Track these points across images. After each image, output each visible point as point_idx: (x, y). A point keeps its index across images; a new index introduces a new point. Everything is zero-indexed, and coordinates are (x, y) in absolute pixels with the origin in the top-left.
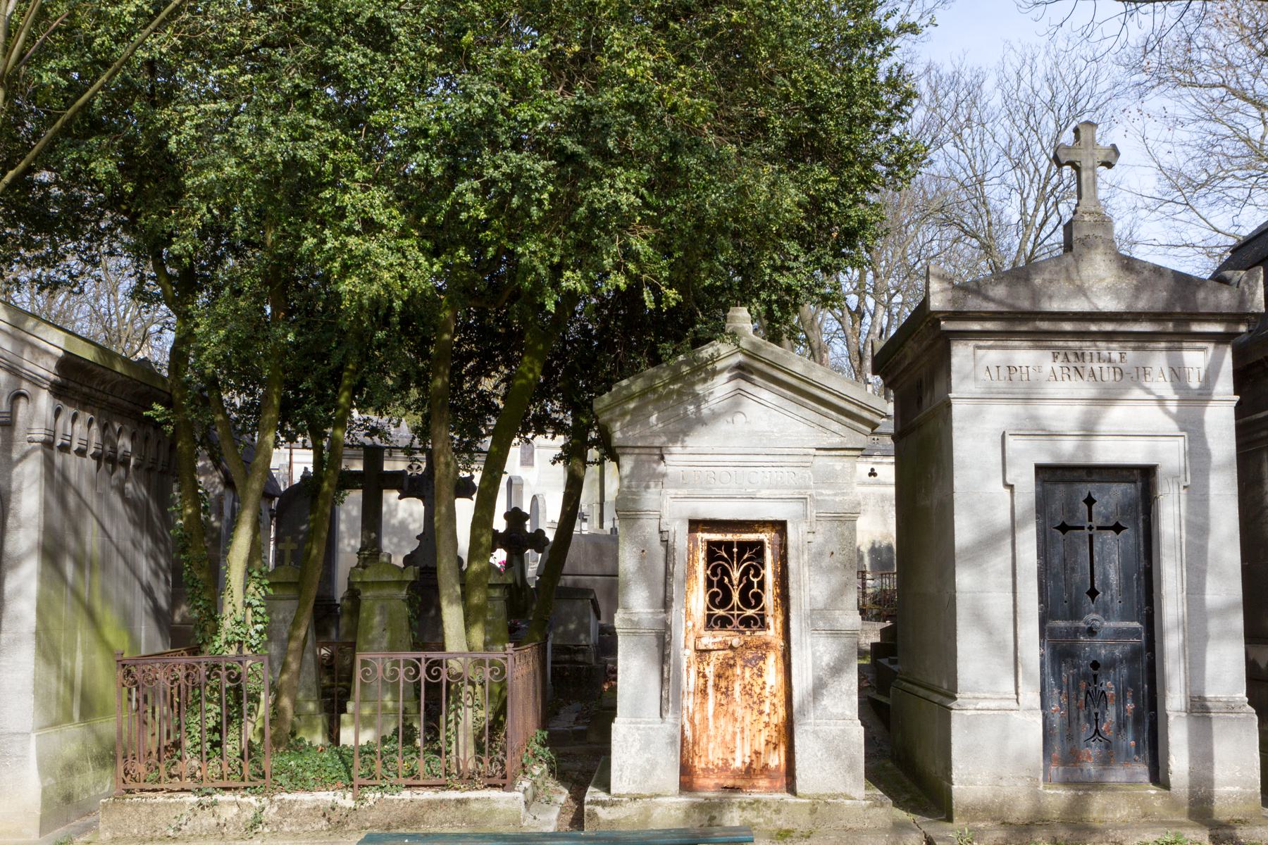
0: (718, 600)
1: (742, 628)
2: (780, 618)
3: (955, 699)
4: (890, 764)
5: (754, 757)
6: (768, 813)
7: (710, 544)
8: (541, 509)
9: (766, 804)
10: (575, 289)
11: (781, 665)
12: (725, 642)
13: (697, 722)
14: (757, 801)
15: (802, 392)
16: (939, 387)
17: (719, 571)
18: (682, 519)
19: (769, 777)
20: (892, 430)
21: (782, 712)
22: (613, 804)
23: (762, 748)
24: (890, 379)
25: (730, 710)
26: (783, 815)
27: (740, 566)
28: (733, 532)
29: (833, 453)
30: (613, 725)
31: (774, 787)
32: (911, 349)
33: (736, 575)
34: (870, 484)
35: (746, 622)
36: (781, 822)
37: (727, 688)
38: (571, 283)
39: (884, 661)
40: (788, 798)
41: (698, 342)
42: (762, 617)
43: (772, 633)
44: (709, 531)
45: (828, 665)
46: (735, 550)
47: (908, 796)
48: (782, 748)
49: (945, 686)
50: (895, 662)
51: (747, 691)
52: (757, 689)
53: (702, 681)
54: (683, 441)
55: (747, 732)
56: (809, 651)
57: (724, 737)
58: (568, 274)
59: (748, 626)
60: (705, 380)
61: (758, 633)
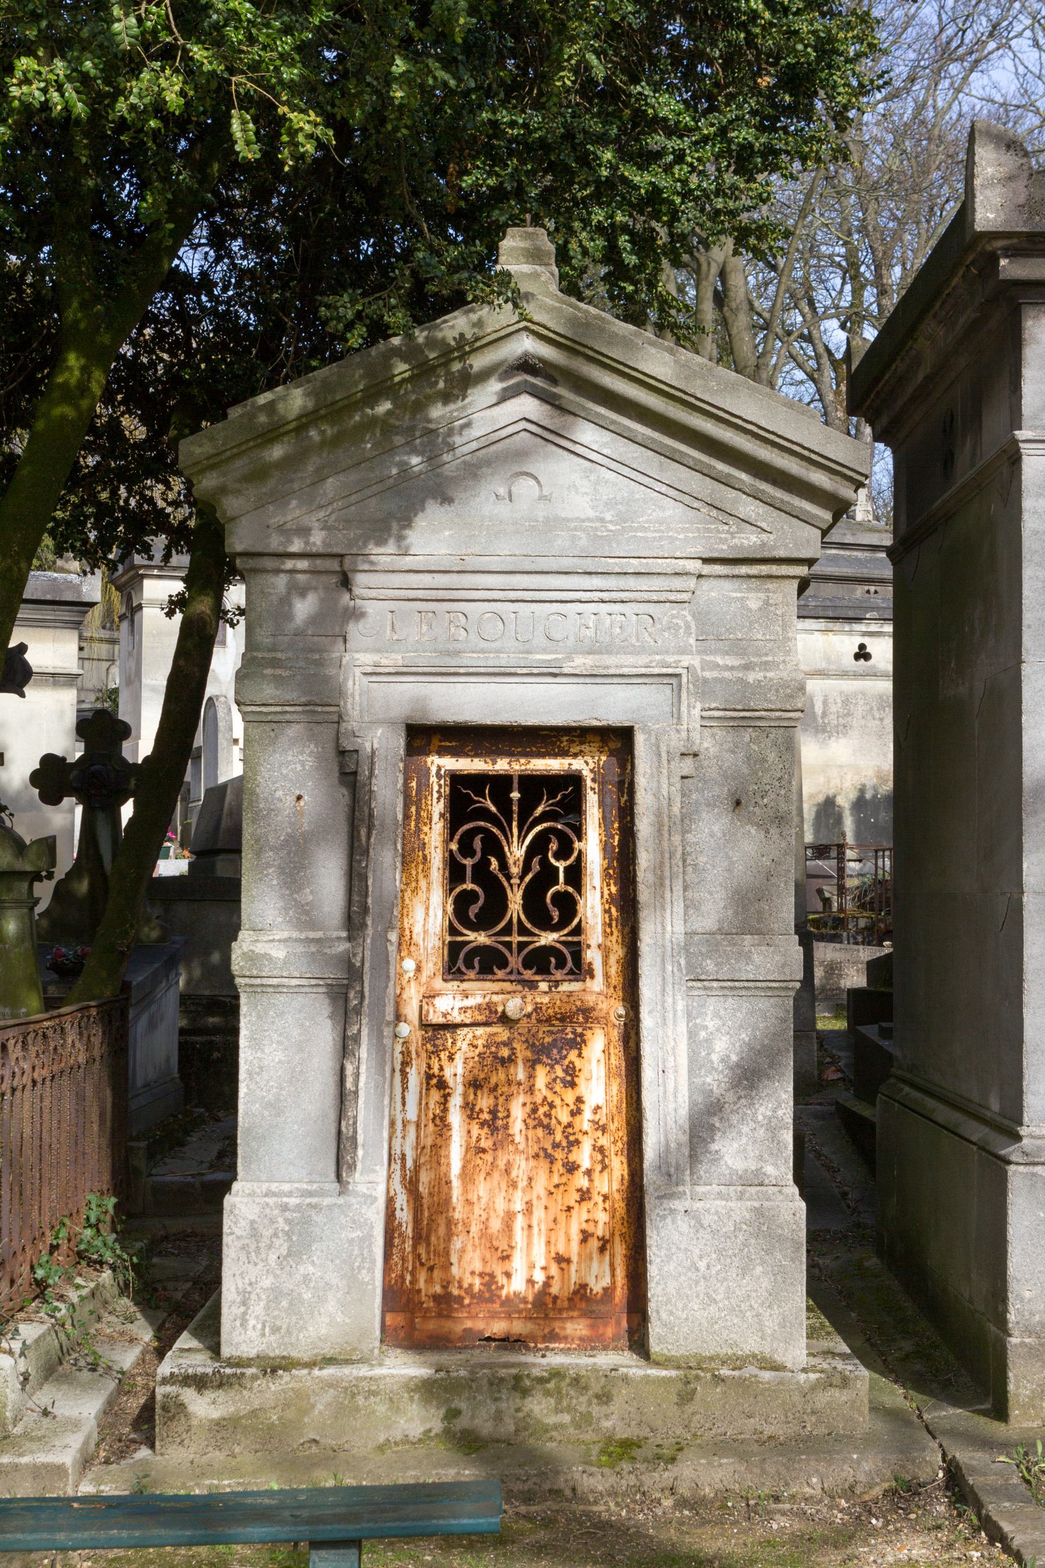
0: (473, 910)
1: (528, 974)
2: (618, 952)
3: (1018, 1138)
4: (873, 1262)
5: (554, 1270)
6: (581, 1403)
7: (457, 779)
8: (221, 724)
9: (576, 1381)
10: (46, 106)
11: (617, 1059)
12: (490, 1007)
13: (423, 1189)
14: (557, 1374)
15: (679, 430)
16: (992, 421)
17: (477, 844)
18: (392, 723)
19: (586, 1314)
20: (888, 540)
21: (619, 1166)
22: (222, 1383)
23: (574, 1250)
24: (884, 420)
25: (501, 1164)
26: (616, 1407)
27: (520, 832)
28: (510, 754)
29: (744, 570)
30: (228, 1200)
31: (600, 1338)
32: (933, 338)
33: (516, 852)
34: (857, 676)
35: (540, 961)
36: (613, 1421)
37: (493, 1112)
38: (34, 92)
39: (870, 1031)
40: (626, 1362)
41: (429, 306)
42: (577, 951)
43: (598, 989)
44: (456, 753)
45: (724, 1060)
46: (515, 795)
47: (908, 1346)
48: (620, 1250)
49: (995, 1105)
50: (886, 1033)
51: (540, 1119)
52: (564, 1117)
53: (435, 1096)
54: (400, 538)
55: (538, 1213)
56: (683, 1028)
57: (486, 1223)
58: (25, 63)
59: (543, 970)
60: (447, 398)
61: (565, 987)
